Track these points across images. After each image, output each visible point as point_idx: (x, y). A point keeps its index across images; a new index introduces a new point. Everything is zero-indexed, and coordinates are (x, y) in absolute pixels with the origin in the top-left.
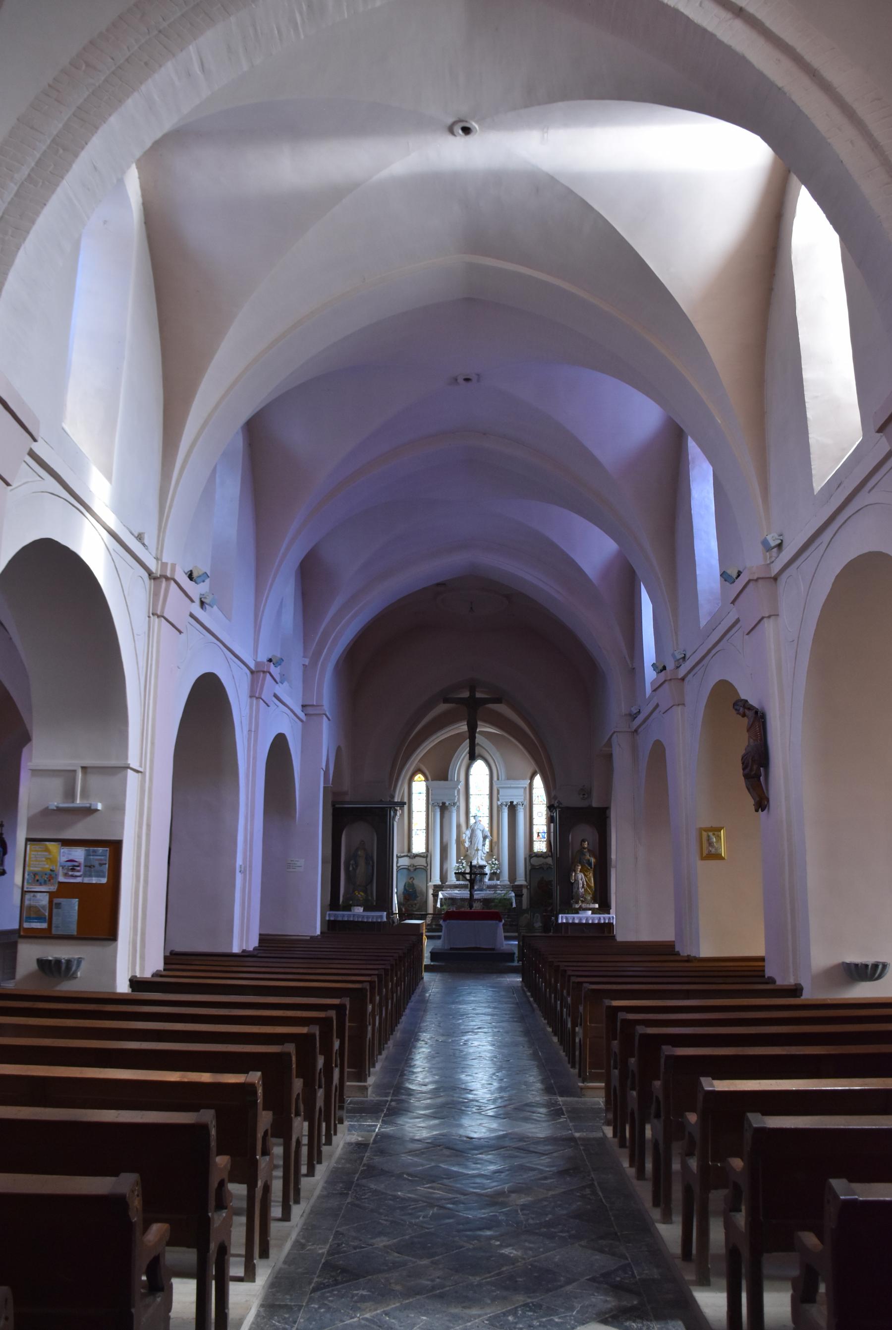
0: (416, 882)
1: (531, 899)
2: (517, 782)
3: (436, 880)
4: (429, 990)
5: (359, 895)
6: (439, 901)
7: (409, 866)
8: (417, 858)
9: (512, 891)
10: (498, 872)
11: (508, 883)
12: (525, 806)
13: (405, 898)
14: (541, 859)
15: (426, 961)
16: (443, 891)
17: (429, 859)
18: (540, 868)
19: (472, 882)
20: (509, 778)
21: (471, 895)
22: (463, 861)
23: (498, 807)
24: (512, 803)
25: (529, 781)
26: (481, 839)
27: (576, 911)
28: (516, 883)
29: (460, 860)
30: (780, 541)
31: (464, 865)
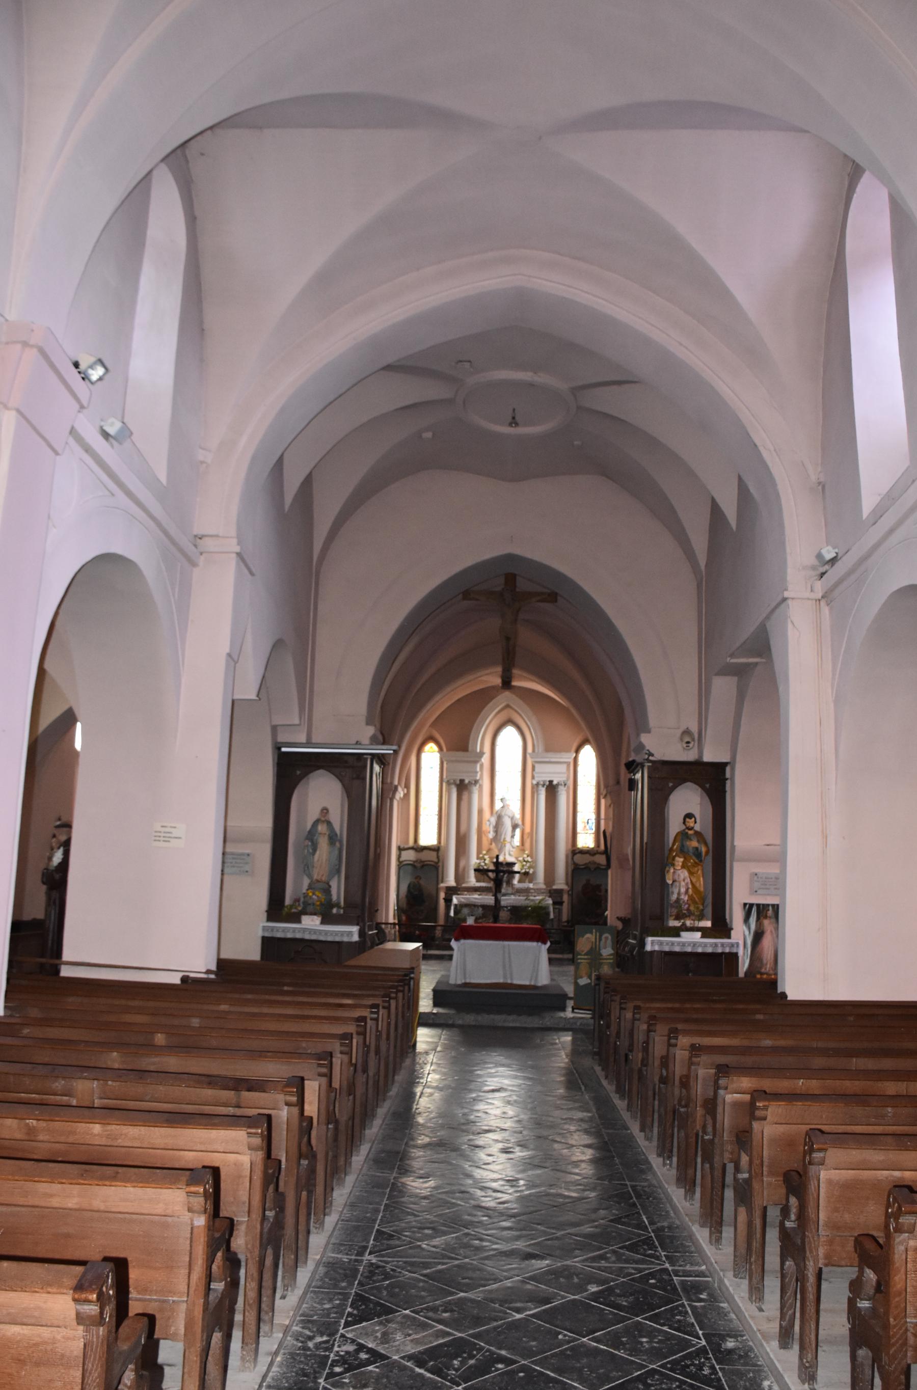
0: (422, 882)
1: (573, 907)
2: (559, 755)
3: (451, 881)
4: (422, 1078)
5: (314, 897)
6: (452, 908)
7: (414, 862)
8: (425, 852)
9: (550, 897)
10: (531, 871)
11: (543, 886)
12: (568, 788)
13: (408, 903)
14: (587, 856)
15: (425, 1005)
16: (458, 895)
17: (440, 853)
18: (585, 868)
19: (498, 883)
20: (548, 749)
21: (497, 901)
22: (486, 857)
23: (533, 788)
24: (551, 782)
25: (574, 755)
26: (510, 829)
27: (676, 932)
28: (555, 887)
29: (481, 856)
30: (835, 555)
31: (487, 862)
